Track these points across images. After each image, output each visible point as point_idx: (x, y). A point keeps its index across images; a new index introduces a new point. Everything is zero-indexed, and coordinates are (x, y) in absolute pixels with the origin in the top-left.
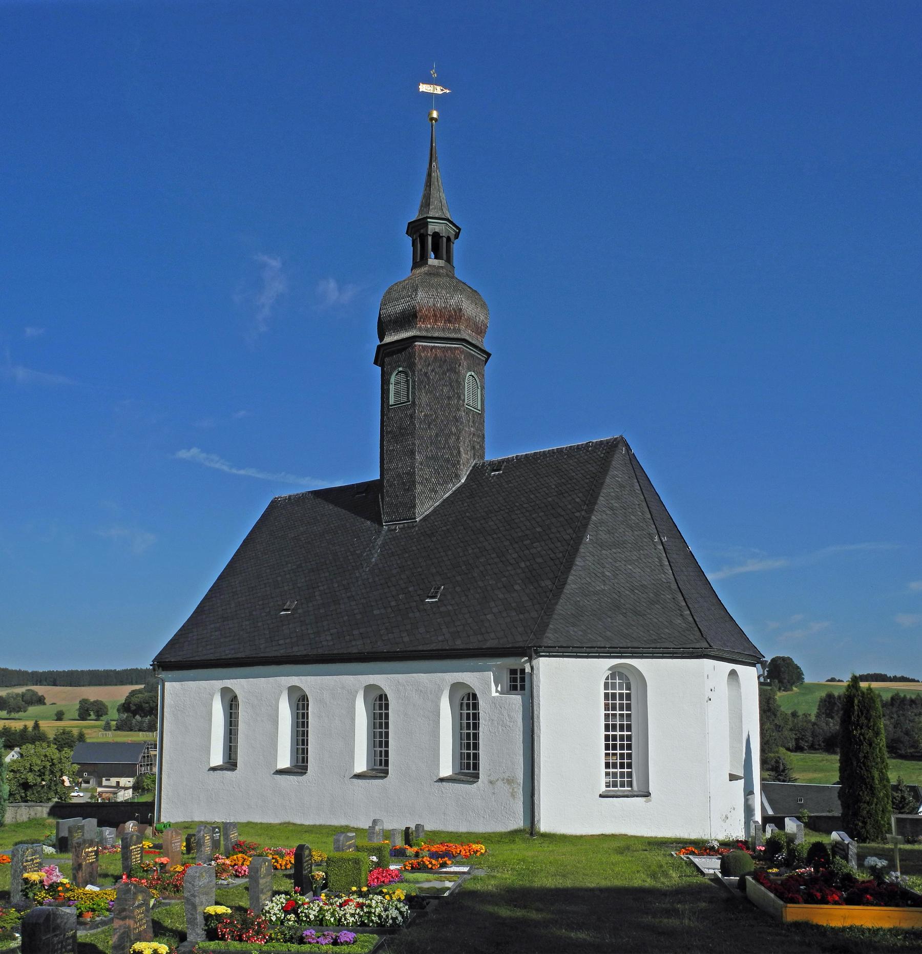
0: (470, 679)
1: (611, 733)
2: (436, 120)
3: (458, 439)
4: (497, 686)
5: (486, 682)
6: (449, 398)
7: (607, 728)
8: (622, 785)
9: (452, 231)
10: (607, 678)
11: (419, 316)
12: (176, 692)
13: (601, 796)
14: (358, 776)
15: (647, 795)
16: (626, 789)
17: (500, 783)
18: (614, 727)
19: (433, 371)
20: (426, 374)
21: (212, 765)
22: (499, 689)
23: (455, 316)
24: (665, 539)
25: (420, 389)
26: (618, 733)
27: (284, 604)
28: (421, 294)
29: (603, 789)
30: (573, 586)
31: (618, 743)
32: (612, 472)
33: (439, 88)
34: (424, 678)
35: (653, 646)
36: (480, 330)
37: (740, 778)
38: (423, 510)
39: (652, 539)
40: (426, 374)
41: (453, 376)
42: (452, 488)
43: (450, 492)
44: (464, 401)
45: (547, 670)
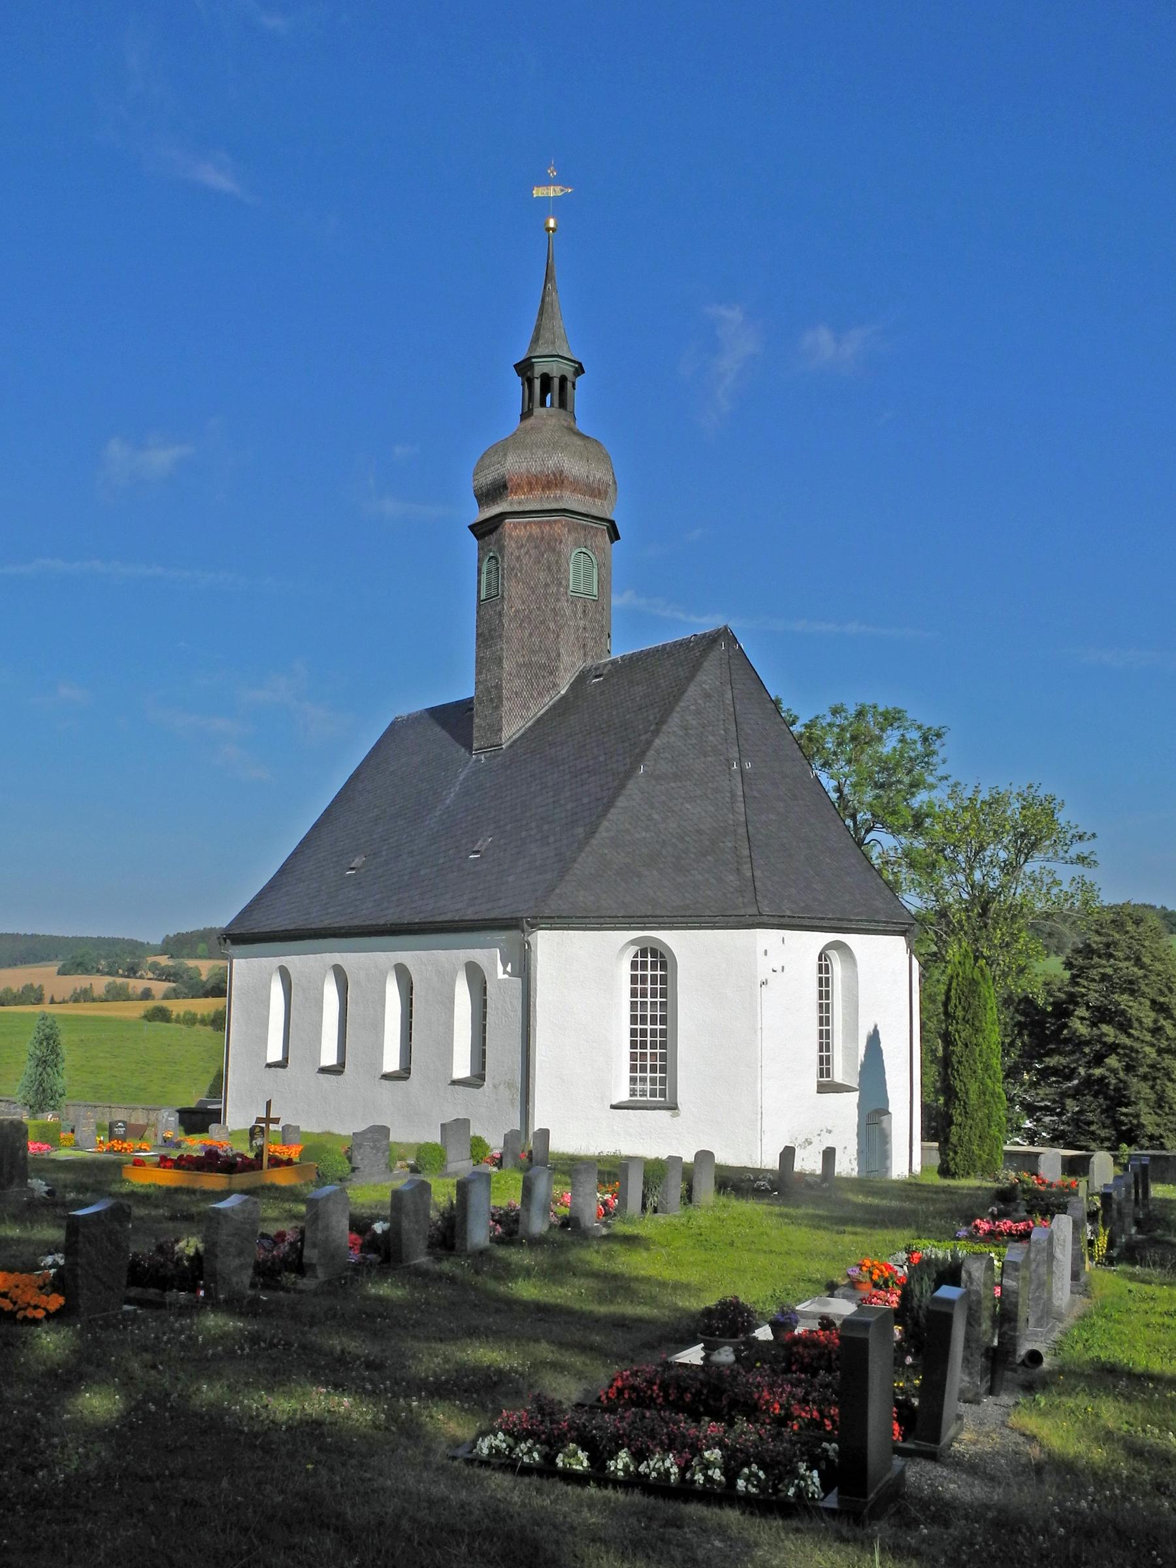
0: (478, 955)
1: (639, 1027)
2: (554, 230)
3: (558, 636)
4: (505, 966)
5: (493, 960)
6: (547, 585)
7: (634, 1019)
8: (653, 1094)
9: (568, 369)
10: (636, 956)
11: (509, 485)
12: (245, 969)
13: (613, 1107)
14: (386, 1077)
15: (673, 1107)
16: (658, 1099)
17: (502, 1087)
18: (643, 1019)
19: (526, 553)
20: (518, 558)
21: (270, 1060)
22: (509, 969)
23: (555, 481)
24: (748, 766)
25: (509, 579)
26: (649, 1027)
27: (475, 842)
28: (510, 459)
29: (624, 1096)
30: (604, 834)
31: (649, 1039)
32: (701, 677)
33: (558, 188)
34: (441, 954)
35: (683, 913)
36: (596, 491)
37: (854, 1090)
38: (511, 730)
39: (730, 765)
40: (518, 558)
41: (553, 559)
42: (548, 701)
43: (546, 708)
44: (567, 586)
45: (550, 947)
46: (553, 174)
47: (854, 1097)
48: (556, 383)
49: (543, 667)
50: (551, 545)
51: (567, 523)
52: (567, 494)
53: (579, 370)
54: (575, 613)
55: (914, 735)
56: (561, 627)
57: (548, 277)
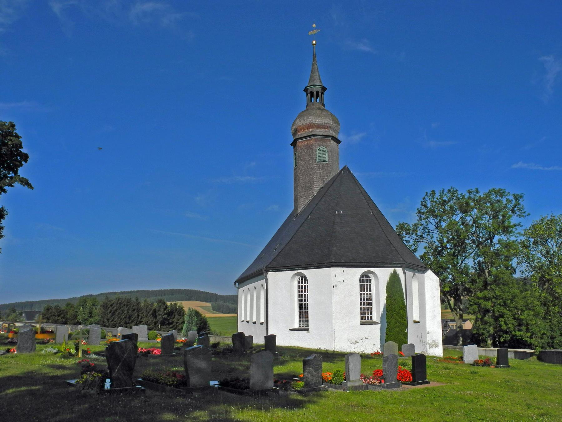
13: (290, 330)
15: (307, 330)
23: (312, 126)
29: (296, 326)
46: (314, 26)
47: (379, 326)
48: (315, 93)
49: (308, 187)
50: (309, 147)
51: (315, 139)
52: (315, 129)
53: (324, 89)
54: (319, 168)
55: (511, 197)
56: (314, 173)
57: (314, 60)
